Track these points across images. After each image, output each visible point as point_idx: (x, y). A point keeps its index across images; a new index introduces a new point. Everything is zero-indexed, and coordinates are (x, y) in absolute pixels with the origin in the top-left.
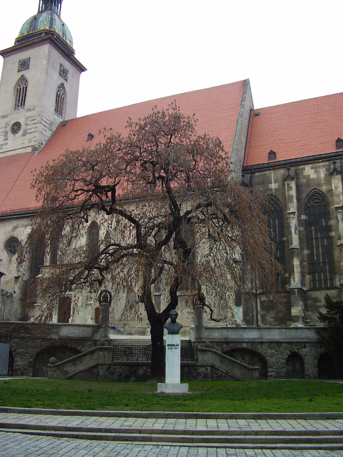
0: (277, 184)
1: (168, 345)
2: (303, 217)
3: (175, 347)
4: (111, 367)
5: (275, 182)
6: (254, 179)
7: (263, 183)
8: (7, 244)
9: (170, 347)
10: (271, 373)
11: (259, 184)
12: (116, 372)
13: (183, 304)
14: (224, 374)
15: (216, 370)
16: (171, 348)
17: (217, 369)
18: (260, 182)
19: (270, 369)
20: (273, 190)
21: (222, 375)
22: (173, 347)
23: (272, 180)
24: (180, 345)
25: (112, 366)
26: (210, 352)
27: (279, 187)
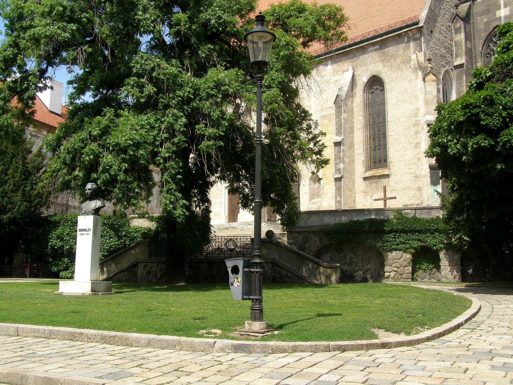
0: (508, 9)
1: (80, 230)
2: (134, 56)
3: (87, 232)
4: (147, 265)
6: (476, 9)
7: (488, 11)
8: (374, 139)
9: (82, 232)
10: (389, 274)
11: (482, 13)
12: (153, 272)
13: (373, 188)
15: (279, 269)
16: (83, 234)
17: (281, 268)
18: (483, 11)
20: (502, 18)
21: (287, 275)
22: (84, 233)
23: (501, 4)
24: (92, 230)
25: (149, 264)
26: (268, 244)
27: (510, 12)
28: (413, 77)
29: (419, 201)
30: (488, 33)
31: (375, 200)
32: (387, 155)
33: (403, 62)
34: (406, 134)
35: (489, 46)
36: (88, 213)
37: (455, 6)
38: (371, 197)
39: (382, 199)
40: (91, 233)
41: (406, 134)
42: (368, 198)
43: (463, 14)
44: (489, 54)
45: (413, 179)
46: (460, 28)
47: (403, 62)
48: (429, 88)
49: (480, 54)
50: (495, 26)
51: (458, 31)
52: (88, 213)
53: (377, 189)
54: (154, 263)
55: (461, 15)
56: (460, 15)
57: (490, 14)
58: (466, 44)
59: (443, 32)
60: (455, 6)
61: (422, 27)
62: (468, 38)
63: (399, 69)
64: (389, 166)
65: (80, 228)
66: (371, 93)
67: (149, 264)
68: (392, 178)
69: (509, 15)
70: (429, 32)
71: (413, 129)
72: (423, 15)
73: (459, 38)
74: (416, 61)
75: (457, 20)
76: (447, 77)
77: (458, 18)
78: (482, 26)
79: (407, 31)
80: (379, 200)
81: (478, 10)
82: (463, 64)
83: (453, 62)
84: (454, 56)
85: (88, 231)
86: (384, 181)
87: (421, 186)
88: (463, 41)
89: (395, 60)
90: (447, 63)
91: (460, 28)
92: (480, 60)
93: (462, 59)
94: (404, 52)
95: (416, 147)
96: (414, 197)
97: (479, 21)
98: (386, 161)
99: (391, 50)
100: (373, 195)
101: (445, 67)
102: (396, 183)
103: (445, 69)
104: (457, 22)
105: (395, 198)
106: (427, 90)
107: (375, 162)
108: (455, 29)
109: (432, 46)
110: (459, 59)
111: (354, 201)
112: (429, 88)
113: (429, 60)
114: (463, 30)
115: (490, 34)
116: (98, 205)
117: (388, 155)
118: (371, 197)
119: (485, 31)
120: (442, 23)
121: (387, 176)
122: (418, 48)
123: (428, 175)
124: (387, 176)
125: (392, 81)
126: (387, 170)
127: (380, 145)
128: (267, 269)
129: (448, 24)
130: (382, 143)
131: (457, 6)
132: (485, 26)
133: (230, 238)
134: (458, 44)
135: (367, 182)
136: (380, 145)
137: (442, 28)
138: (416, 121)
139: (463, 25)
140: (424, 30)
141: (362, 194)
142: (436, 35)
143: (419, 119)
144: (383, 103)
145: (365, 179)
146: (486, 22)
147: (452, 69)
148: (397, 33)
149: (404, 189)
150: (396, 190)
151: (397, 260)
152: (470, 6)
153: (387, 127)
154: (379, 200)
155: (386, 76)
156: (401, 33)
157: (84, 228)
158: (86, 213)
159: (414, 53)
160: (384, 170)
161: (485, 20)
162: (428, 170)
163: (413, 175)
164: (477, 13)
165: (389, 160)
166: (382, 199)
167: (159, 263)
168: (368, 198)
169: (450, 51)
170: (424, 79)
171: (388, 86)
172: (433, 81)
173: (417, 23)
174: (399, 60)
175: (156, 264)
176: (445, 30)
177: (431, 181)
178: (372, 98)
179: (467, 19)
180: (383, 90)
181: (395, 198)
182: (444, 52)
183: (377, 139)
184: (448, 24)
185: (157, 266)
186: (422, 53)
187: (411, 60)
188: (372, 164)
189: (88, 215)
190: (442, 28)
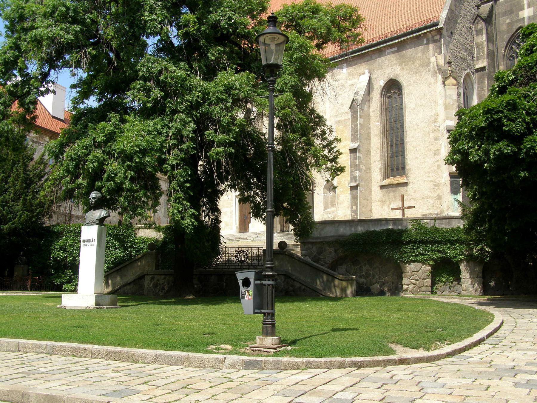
0: (531, 9)
1: (84, 241)
2: (141, 58)
3: (91, 243)
4: (154, 277)
5: (529, 6)
6: (498, 9)
7: (511, 12)
8: (391, 146)
9: (86, 243)
10: (407, 286)
11: (505, 14)
12: (160, 285)
13: (391, 197)
14: (303, 287)
15: (292, 281)
16: (86, 245)
17: (294, 280)
18: (505, 12)
19: (405, 281)
20: (526, 19)
21: (300, 288)
22: (88, 243)
23: (524, 4)
24: (96, 241)
25: (156, 276)
26: (281, 256)
27: (534, 12)
28: (432, 80)
29: (439, 211)
30: (510, 34)
31: (393, 209)
32: (405, 163)
33: (421, 65)
34: (425, 141)
35: (512, 48)
36: (92, 223)
37: (476, 6)
38: (389, 206)
39: (400, 209)
40: (95, 244)
41: (425, 141)
42: (386, 207)
43: (484, 15)
44: (512, 56)
45: (433, 187)
46: (481, 29)
47: (421, 65)
48: (449, 92)
49: (502, 57)
50: (518, 27)
51: (479, 32)
52: (92, 223)
53: (395, 197)
54: (161, 275)
55: (482, 16)
56: (481, 16)
57: (513, 15)
58: (488, 46)
59: (463, 34)
60: (476, 6)
61: (442, 28)
62: (490, 39)
63: (417, 72)
64: (408, 174)
65: (84, 239)
66: (388, 98)
67: (156, 276)
68: (410, 187)
69: (533, 16)
70: (449, 34)
71: (432, 135)
72: (443, 16)
73: (481, 40)
74: (435, 64)
75: (479, 21)
76: (468, 80)
77: (480, 19)
78: (504, 28)
79: (426, 33)
80: (396, 209)
81: (500, 10)
82: (485, 67)
83: (474, 65)
84: (475, 59)
85: (92, 242)
86: (402, 189)
87: (441, 194)
88: (485, 43)
89: (413, 63)
90: (468, 66)
91: (481, 29)
92: (502, 63)
93: (483, 61)
94: (423, 55)
95: (435, 154)
96: (433, 206)
97: (501, 22)
98: (404, 168)
99: (409, 52)
100: (390, 204)
101: (465, 70)
102: (415, 192)
103: (466, 72)
104: (478, 23)
105: (414, 207)
106: (447, 94)
107: (392, 170)
108: (476, 31)
109: (453, 48)
110: (480, 62)
111: (371, 210)
112: (449, 92)
113: (449, 63)
114: (484, 31)
115: (513, 35)
116: (102, 214)
117: (406, 162)
118: (389, 206)
119: (508, 33)
120: (463, 24)
121: (406, 184)
122: (438, 51)
123: (448, 183)
124: (406, 184)
125: (410, 84)
126: (405, 178)
127: (397, 152)
128: (279, 282)
129: (469, 25)
130: (400, 149)
131: (478, 7)
132: (508, 27)
133: (241, 249)
134: (479, 46)
135: (384, 190)
136: (397, 152)
137: (463, 29)
138: (436, 126)
139: (484, 27)
140: (444, 32)
141: (379, 203)
142: (456, 36)
143: (438, 124)
144: (401, 108)
145: (382, 187)
146: (509, 23)
147: (473, 72)
148: (415, 34)
149: (423, 198)
150: (414, 199)
151: (416, 273)
152: (492, 6)
153: (405, 133)
154: (396, 209)
155: (404, 79)
156: (420, 35)
157: (88, 239)
158: (90, 223)
159: (434, 55)
160: (402, 178)
161: (508, 21)
162: (448, 178)
163: (432, 184)
164: (499, 13)
165: (407, 167)
166: (400, 209)
167: (166, 275)
168: (386, 207)
169: (471, 53)
170: (444, 83)
171: (406, 91)
172: (453, 85)
173: (437, 24)
174: (417, 63)
175: (163, 277)
176: (466, 31)
177: (451, 190)
178: (390, 102)
179: (489, 20)
180: (401, 94)
181: (414, 207)
182: (465, 54)
183: (394, 146)
184: (469, 25)
185: (165, 278)
186: (442, 55)
187: (430, 63)
188: (390, 171)
189: (93, 225)
190: (463, 29)
